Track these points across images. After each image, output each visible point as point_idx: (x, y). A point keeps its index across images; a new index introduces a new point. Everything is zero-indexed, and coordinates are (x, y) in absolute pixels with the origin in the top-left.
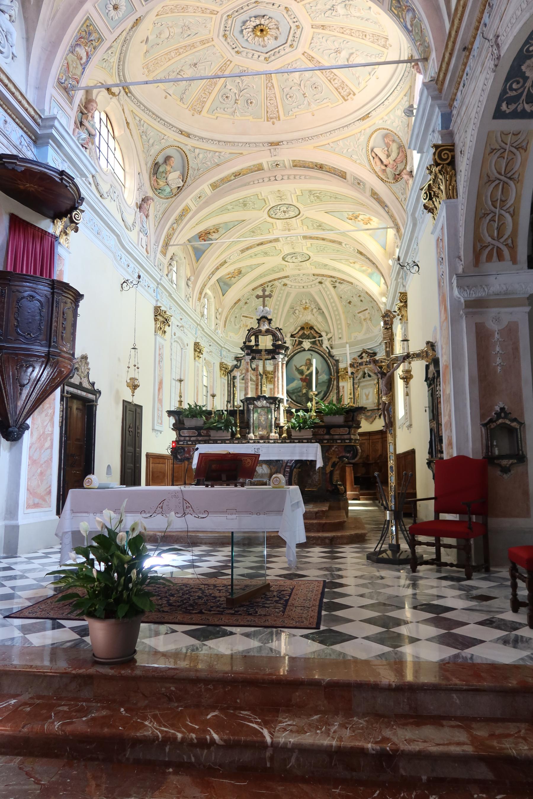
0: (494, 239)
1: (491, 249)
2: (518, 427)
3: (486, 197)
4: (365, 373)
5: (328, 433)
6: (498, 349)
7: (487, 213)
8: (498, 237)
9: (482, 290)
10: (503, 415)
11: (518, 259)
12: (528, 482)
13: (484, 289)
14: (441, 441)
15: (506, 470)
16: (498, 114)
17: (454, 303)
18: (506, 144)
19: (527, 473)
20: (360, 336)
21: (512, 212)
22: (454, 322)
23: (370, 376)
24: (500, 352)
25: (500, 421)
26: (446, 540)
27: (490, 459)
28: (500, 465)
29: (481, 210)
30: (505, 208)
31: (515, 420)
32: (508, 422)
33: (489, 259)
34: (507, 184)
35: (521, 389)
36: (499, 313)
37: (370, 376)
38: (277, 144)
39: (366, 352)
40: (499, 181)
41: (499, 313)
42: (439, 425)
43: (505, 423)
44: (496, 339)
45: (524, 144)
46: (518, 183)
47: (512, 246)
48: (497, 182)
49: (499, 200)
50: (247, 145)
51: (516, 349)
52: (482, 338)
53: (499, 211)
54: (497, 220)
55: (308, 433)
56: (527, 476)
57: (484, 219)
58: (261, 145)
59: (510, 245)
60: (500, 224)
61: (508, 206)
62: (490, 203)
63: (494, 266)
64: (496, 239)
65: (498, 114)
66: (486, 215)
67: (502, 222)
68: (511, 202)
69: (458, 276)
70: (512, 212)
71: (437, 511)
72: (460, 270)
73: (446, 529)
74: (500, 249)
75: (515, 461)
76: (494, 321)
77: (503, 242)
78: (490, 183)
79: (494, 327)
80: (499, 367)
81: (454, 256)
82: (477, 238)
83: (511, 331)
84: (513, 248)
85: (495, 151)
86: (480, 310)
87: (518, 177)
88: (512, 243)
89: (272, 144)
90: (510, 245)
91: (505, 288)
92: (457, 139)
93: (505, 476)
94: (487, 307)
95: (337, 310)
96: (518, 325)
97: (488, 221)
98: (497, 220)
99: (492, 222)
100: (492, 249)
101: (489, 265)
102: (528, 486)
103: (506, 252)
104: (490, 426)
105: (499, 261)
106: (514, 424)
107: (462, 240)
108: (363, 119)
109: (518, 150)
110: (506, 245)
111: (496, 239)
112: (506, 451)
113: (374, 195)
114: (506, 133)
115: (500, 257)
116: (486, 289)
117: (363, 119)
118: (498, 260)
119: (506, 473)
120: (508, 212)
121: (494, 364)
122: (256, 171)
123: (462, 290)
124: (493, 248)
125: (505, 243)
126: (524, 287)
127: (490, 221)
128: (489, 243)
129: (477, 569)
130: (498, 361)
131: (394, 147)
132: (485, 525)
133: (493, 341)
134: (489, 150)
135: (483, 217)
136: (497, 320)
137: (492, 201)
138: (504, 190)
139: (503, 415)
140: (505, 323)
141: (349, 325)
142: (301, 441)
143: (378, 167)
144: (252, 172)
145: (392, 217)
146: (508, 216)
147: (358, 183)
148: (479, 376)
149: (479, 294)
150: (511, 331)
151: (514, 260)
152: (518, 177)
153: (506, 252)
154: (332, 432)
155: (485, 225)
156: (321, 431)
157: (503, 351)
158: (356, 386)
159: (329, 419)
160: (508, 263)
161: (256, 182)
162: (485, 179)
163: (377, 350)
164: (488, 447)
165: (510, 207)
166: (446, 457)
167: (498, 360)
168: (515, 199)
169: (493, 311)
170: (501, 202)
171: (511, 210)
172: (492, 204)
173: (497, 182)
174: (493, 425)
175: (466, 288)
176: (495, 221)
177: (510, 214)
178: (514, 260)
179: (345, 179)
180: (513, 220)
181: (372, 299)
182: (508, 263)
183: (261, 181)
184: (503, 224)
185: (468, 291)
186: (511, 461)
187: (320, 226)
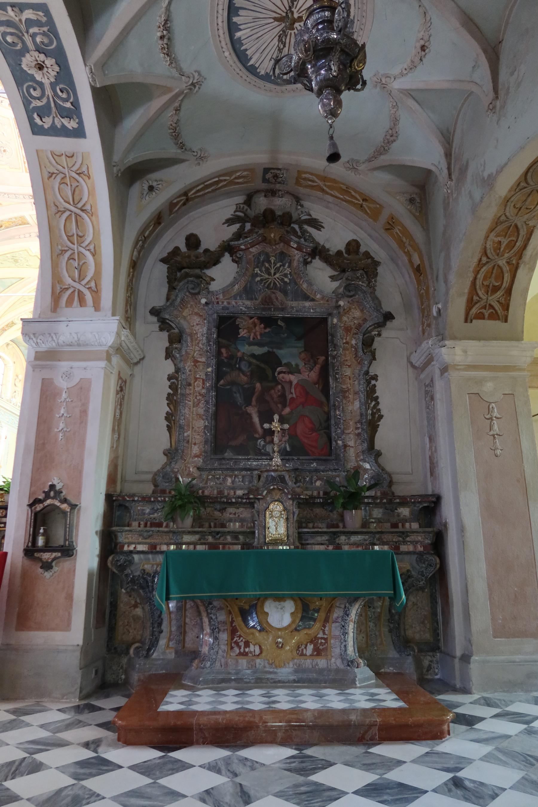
0: (75, 281)
1: (72, 292)
2: (69, 510)
3: (60, 230)
6: (62, 411)
7: (64, 250)
8: (79, 279)
9: (50, 339)
10: (52, 494)
11: (102, 305)
12: (73, 583)
13: (52, 337)
15: (47, 566)
18: (64, 168)
19: (74, 571)
21: (92, 250)
24: (65, 415)
25: (49, 502)
28: (40, 559)
29: (57, 246)
30: (84, 245)
31: (65, 501)
32: (57, 503)
33: (69, 303)
34: (80, 216)
35: (82, 461)
36: (71, 368)
40: (70, 213)
41: (71, 368)
43: (53, 505)
44: (63, 399)
45: (84, 169)
46: (92, 216)
47: (96, 290)
48: (67, 214)
49: (75, 236)
50: (6, 195)
51: (84, 412)
53: (78, 248)
54: (76, 258)
56: (74, 575)
57: (61, 257)
58: (22, 197)
59: (94, 288)
60: (81, 264)
61: (86, 243)
62: (66, 238)
63: (76, 310)
64: (77, 280)
66: (63, 252)
67: (83, 262)
68: (89, 238)
70: (92, 250)
74: (82, 292)
75: (59, 554)
76: (64, 376)
77: (85, 285)
78: (60, 213)
79: (62, 384)
80: (61, 435)
82: (56, 278)
83: (82, 390)
84: (96, 292)
85: (54, 176)
86: (48, 363)
87: (91, 209)
88: (96, 286)
90: (94, 288)
91: (76, 339)
93: (46, 574)
94: (59, 360)
96: (91, 382)
97: (66, 259)
98: (76, 258)
99: (71, 261)
100: (74, 291)
101: (69, 310)
102: (73, 588)
103: (88, 297)
104: (36, 508)
105: (81, 306)
106: (64, 506)
109: (80, 176)
110: (88, 288)
111: (77, 280)
114: (59, 154)
115: (82, 302)
116: (54, 338)
118: (79, 306)
120: (88, 250)
121: (56, 430)
122: (20, 225)
123: (27, 338)
124: (74, 291)
125: (87, 286)
126: (97, 338)
127: (69, 259)
128: (69, 285)
130: (61, 426)
133: (59, 401)
134: (46, 175)
135: (60, 254)
136: (67, 375)
137: (68, 236)
138: (79, 224)
139: (52, 494)
140: (75, 380)
144: (16, 225)
146: (87, 254)
148: (37, 444)
151: (97, 307)
152: (91, 209)
153: (88, 297)
155: (64, 264)
157: (68, 414)
160: (89, 309)
161: (22, 236)
162: (54, 209)
165: (89, 244)
167: (61, 424)
168: (94, 234)
169: (64, 365)
170: (79, 238)
171: (92, 247)
172: (68, 239)
173: (67, 214)
174: (39, 507)
175: (32, 336)
176: (75, 260)
177: (91, 252)
178: (97, 307)
179: (28, 224)
180: (94, 259)
183: (27, 235)
184: (84, 263)
185: (34, 339)
186: (54, 555)
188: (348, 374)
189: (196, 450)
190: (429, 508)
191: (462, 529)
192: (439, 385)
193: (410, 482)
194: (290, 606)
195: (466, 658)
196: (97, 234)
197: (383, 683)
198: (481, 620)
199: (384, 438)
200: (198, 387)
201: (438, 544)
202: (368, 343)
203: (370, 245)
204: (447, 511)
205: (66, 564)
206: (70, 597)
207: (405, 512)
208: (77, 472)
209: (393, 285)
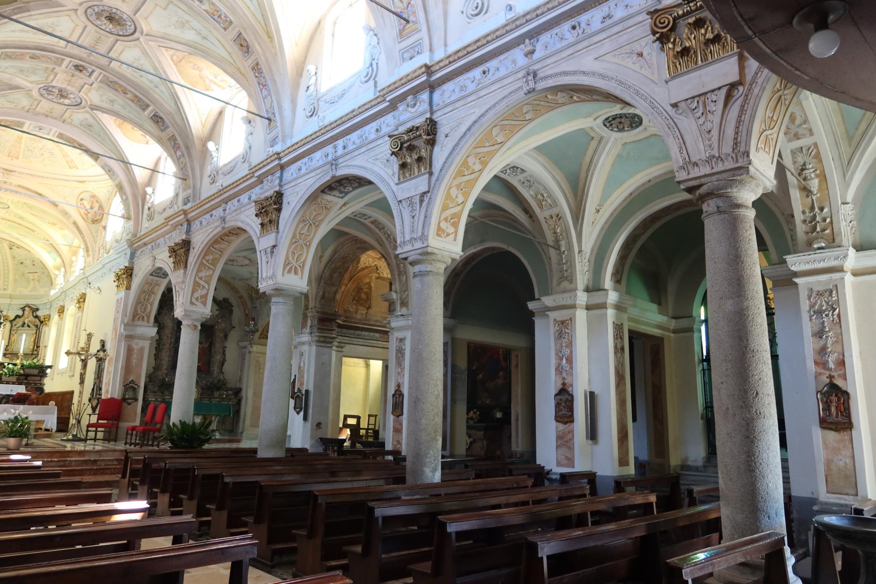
4: (24, 323)
5: (26, 379)
14: (100, 389)
15: (129, 404)
16: (151, 275)
17: (121, 335)
20: (26, 292)
22: (119, 341)
23: (29, 326)
26: (99, 429)
27: (124, 399)
33: (139, 319)
37: (29, 326)
38: (11, 171)
39: (29, 307)
42: (101, 382)
51: (142, 357)
52: (129, 351)
55: (14, 379)
63: (140, 323)
65: (151, 275)
69: (125, 325)
71: (98, 420)
72: (126, 321)
73: (101, 426)
79: (135, 347)
81: (124, 314)
82: (135, 310)
83: (142, 350)
84: (148, 317)
89: (6, 170)
92: (135, 267)
95: (8, 266)
103: (146, 318)
107: (129, 310)
108: (80, 182)
112: (131, 396)
113: (75, 223)
117: (80, 182)
119: (183, 240)
129: (112, 440)
131: (96, 206)
132: (118, 424)
136: (137, 344)
141: (15, 281)
142: (8, 383)
143: (82, 211)
145: (85, 242)
147: (65, 213)
149: (132, 333)
150: (142, 350)
151: (148, 322)
153: (146, 318)
154: (29, 378)
156: (22, 378)
158: (13, 332)
159: (28, 371)
163: (40, 307)
164: (124, 395)
166: (103, 397)
169: (136, 341)
178: (148, 322)
181: (44, 267)
182: (145, 323)
187: (22, 218)
188: (218, 346)
189: (165, 367)
190: (238, 392)
191: (247, 399)
192: (247, 356)
193: (232, 384)
194: (200, 417)
195: (242, 432)
196: (154, 299)
197: (755, 220)
198: (248, 423)
199: (226, 367)
200: (167, 346)
201: (239, 403)
202: (226, 336)
203: (233, 301)
204: (243, 393)
205: (134, 404)
206: (136, 413)
207: (230, 392)
208: (139, 377)
209: (237, 314)
